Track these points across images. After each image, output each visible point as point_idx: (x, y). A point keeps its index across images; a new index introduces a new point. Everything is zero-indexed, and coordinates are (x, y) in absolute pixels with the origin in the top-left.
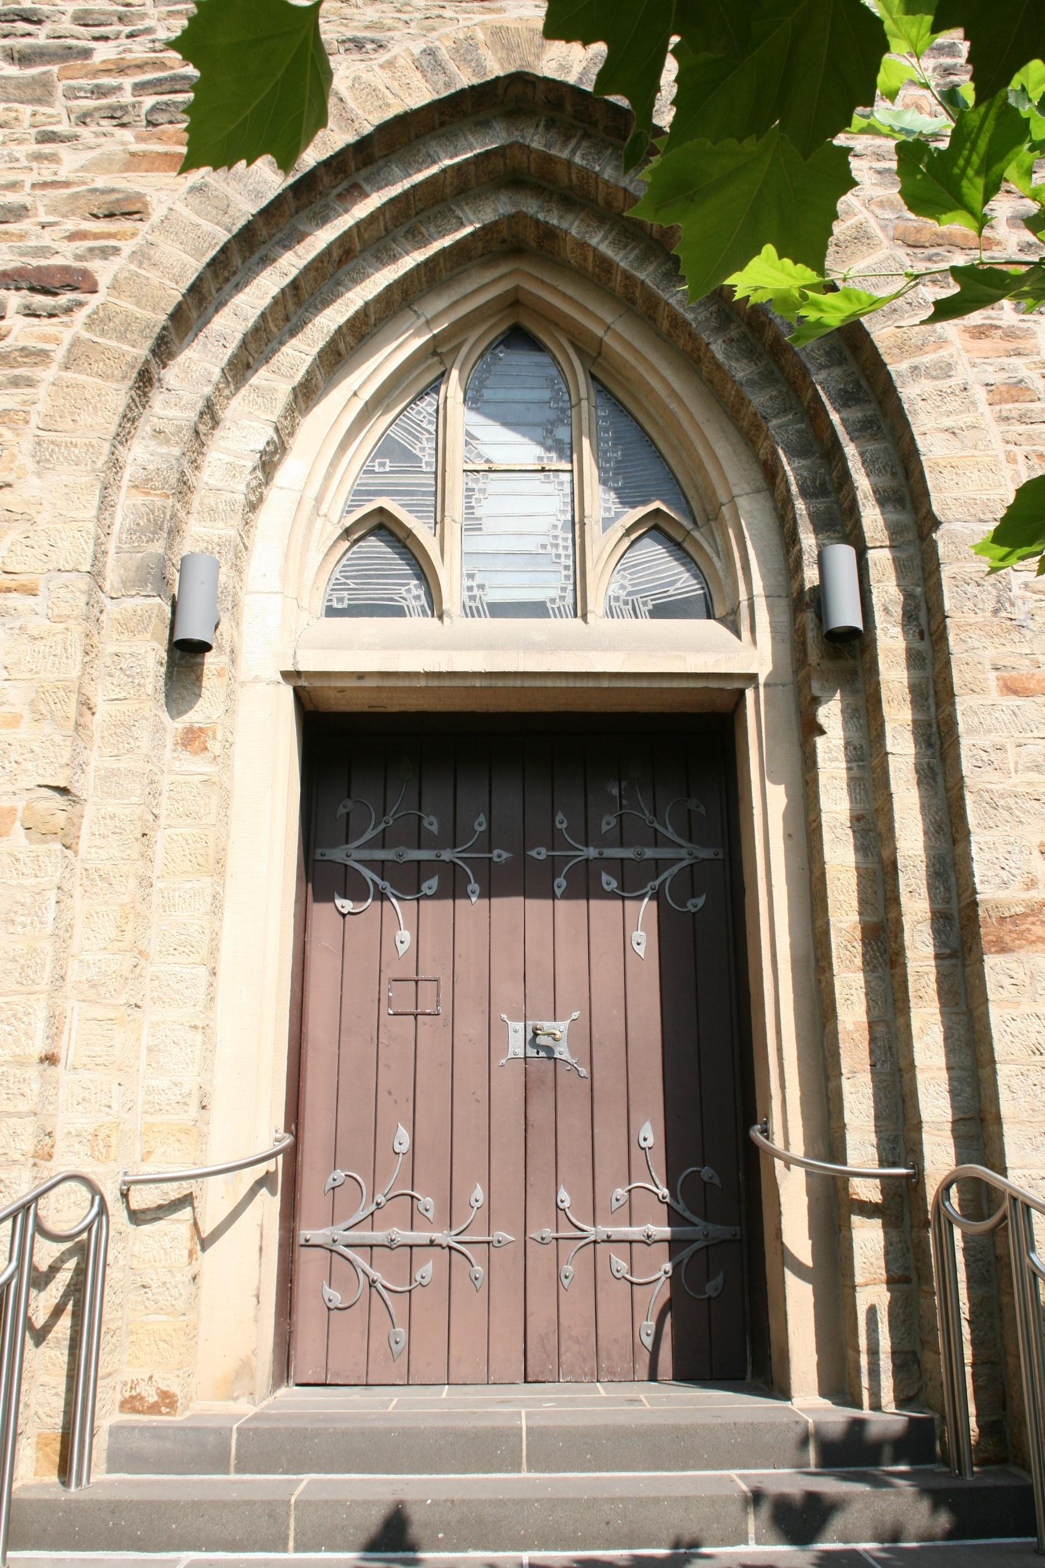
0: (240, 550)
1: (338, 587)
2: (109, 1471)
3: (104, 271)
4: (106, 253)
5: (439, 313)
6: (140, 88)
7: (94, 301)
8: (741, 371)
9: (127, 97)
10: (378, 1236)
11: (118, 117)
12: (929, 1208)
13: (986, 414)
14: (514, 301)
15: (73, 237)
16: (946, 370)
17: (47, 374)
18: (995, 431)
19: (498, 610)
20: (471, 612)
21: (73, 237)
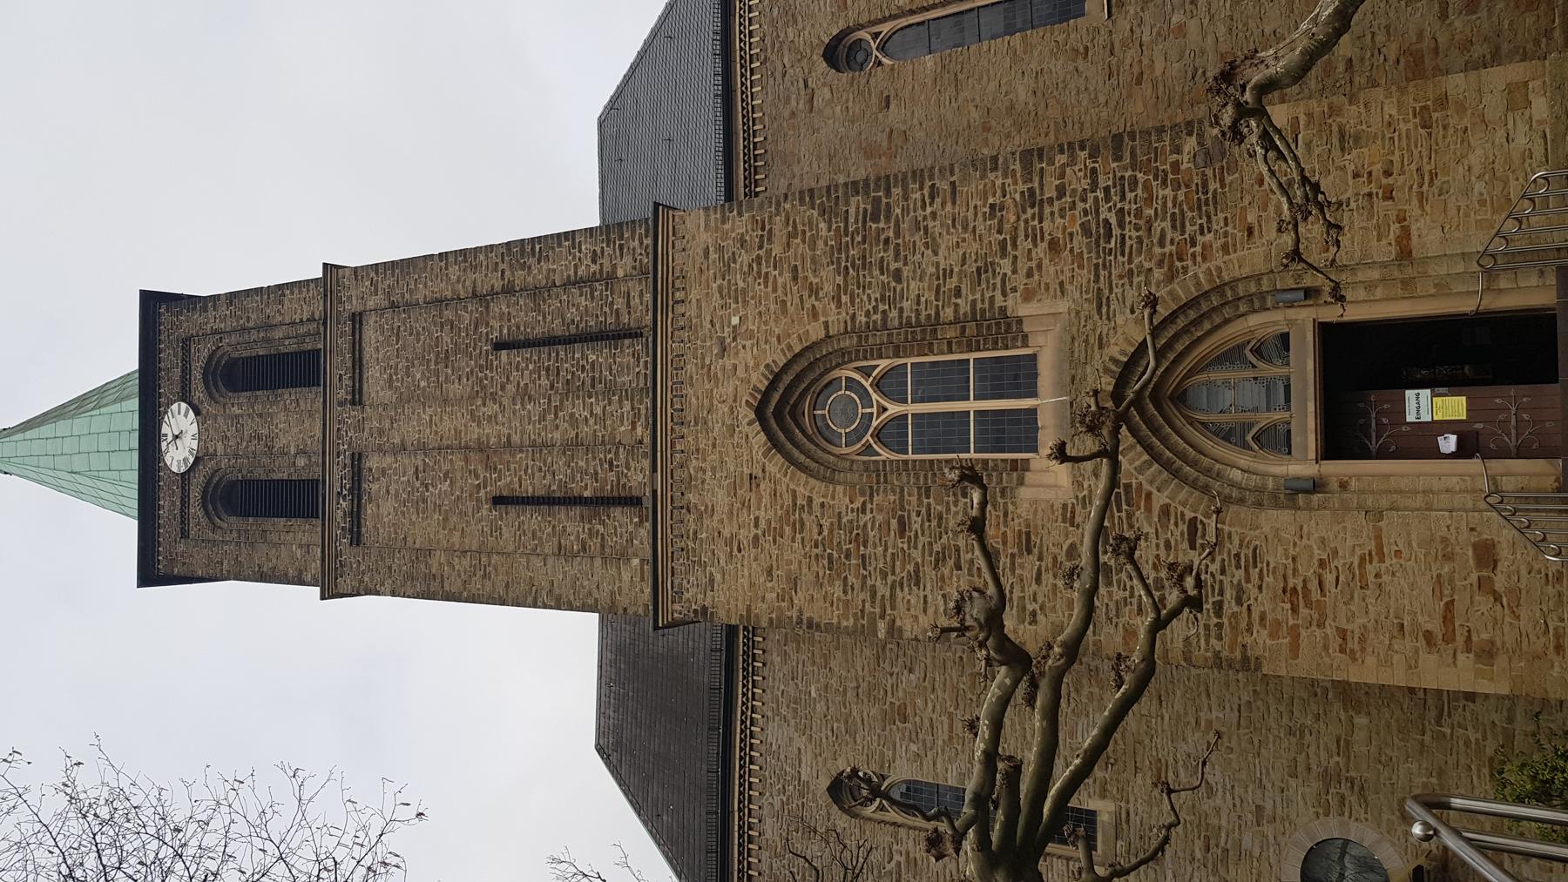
0: (1275, 476)
1: (1280, 451)
2: (1033, 412)
3: (1189, 515)
4: (1183, 514)
5: (1179, 421)
6: (1119, 510)
7: (1200, 517)
8: (1207, 326)
9: (1124, 514)
10: (1513, 432)
11: (1129, 516)
12: (1022, 796)
13: (1233, 256)
14: (1171, 398)
15: (1176, 525)
16: (1219, 269)
17: (1226, 528)
18: (1239, 253)
19: (1288, 399)
20: (1289, 409)
21: (1176, 525)
